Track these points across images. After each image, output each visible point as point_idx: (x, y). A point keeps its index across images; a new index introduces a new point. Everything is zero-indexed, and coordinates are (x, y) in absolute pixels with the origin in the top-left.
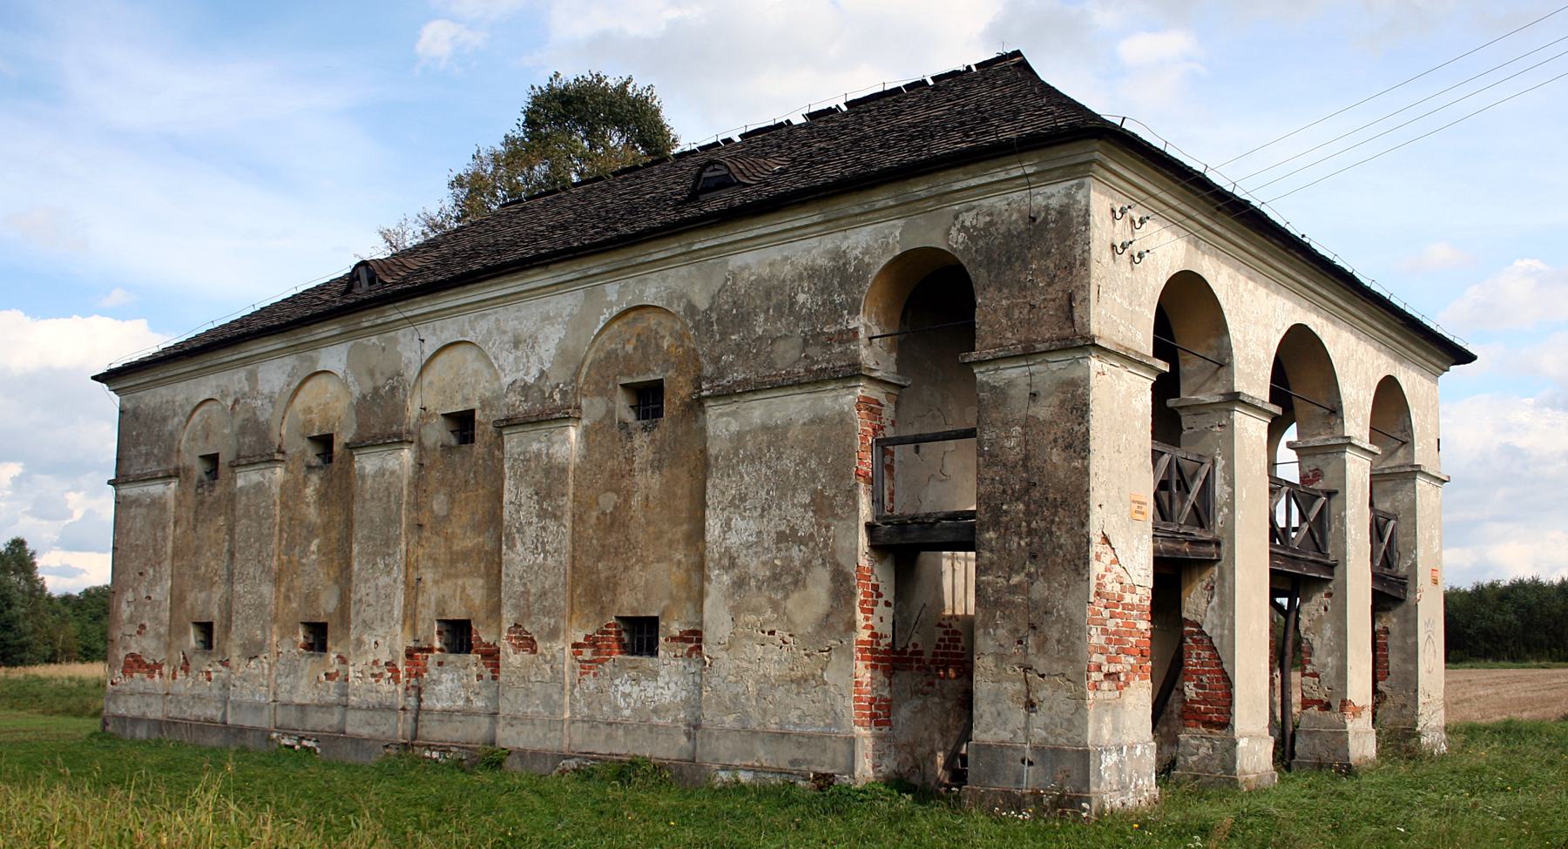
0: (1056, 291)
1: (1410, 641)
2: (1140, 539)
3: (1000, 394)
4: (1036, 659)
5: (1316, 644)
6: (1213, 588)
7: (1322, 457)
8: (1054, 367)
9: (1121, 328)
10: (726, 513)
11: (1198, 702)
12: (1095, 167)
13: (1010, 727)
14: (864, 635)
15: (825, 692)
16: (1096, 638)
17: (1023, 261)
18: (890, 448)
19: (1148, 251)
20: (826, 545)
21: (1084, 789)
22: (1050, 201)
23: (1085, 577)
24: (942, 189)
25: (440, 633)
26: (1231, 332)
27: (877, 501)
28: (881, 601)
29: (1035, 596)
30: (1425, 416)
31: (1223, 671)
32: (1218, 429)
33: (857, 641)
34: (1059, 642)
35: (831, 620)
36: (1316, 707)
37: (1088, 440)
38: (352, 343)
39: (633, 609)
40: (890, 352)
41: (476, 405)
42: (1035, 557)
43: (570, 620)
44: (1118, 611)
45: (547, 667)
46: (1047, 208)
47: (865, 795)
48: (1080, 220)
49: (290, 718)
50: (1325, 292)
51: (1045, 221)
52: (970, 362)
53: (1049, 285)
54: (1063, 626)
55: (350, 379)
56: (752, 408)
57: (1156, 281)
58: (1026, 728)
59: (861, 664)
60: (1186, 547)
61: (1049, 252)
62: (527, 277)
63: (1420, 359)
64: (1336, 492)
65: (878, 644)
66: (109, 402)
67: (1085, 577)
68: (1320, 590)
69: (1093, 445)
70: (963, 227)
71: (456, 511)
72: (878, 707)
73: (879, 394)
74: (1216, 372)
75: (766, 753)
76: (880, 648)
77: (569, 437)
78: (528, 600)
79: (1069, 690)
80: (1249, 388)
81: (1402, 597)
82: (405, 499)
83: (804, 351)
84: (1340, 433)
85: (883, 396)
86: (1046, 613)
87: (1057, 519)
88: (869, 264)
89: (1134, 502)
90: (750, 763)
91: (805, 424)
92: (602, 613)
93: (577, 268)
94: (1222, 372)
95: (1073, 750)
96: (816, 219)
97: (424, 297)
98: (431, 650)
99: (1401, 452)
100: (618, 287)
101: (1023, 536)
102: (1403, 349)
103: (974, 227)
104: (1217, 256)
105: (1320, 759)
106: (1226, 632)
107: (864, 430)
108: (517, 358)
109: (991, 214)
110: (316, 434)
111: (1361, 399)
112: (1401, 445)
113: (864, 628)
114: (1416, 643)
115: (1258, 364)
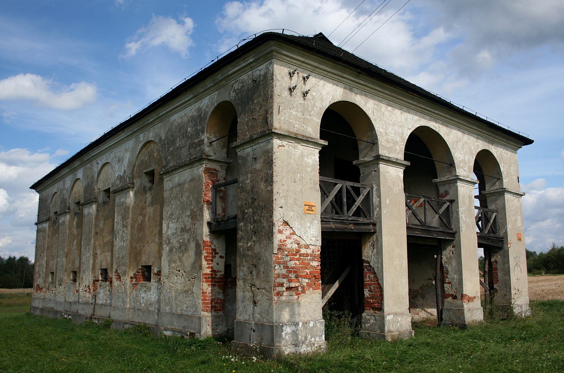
0: (262, 112)
1: (506, 266)
2: (311, 223)
3: (244, 159)
4: (256, 281)
5: (449, 269)
6: (374, 245)
7: (447, 185)
8: (262, 145)
9: (296, 126)
10: (168, 221)
11: (370, 298)
12: (274, 53)
13: (248, 313)
14: (208, 271)
15: (193, 296)
16: (278, 270)
17: (252, 100)
18: (223, 188)
19: (309, 90)
20: (194, 232)
21: (272, 344)
22: (261, 72)
23: (272, 242)
24: (226, 75)
25: (101, 274)
26: (376, 129)
27: (214, 213)
28: (217, 256)
29: (256, 251)
30: (509, 167)
31: (379, 284)
32: (374, 172)
33: (203, 274)
34: (263, 272)
35: (195, 265)
36: (451, 298)
37: (273, 176)
38: (84, 167)
39: (145, 263)
40: (222, 149)
41: (111, 186)
42: (255, 233)
43: (129, 267)
44: (296, 257)
45: (123, 287)
46: (260, 75)
47: (204, 345)
48: (270, 78)
49: (67, 307)
50: (437, 112)
51: (259, 81)
52: (233, 147)
53: (260, 109)
54: (265, 265)
55: (83, 180)
56: (175, 177)
57: (322, 105)
58: (253, 314)
59: (205, 284)
60: (352, 227)
61: (261, 94)
62: (119, 135)
63: (504, 143)
64: (454, 201)
65: (217, 275)
66: (35, 197)
67: (272, 242)
68: (450, 245)
69: (275, 179)
70: (234, 90)
71: (105, 227)
72: (216, 303)
73: (216, 167)
74: (372, 147)
75: (177, 323)
76: (217, 277)
77: (130, 195)
78: (119, 260)
79: (267, 296)
80: (389, 153)
81: (501, 246)
82: (93, 223)
83: (189, 151)
84: (455, 174)
85: (219, 167)
86: (259, 259)
87: (263, 215)
88: (208, 112)
89: (305, 205)
90: (172, 328)
91: (189, 182)
92: (137, 265)
93: (131, 129)
94: (374, 147)
95: (268, 325)
96: (191, 96)
97: (97, 147)
98: (98, 281)
99: (497, 183)
100: (143, 135)
101: (252, 223)
102: (492, 138)
103: (237, 89)
104: (366, 96)
105: (452, 321)
106: (380, 265)
107: (206, 182)
108: (119, 166)
109: (243, 83)
110: (77, 202)
111: (467, 159)
112: (497, 180)
113: (208, 268)
114: (509, 267)
115: (396, 143)
